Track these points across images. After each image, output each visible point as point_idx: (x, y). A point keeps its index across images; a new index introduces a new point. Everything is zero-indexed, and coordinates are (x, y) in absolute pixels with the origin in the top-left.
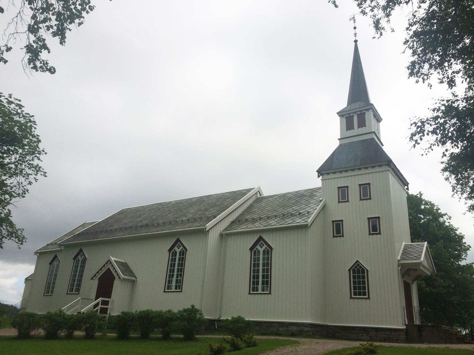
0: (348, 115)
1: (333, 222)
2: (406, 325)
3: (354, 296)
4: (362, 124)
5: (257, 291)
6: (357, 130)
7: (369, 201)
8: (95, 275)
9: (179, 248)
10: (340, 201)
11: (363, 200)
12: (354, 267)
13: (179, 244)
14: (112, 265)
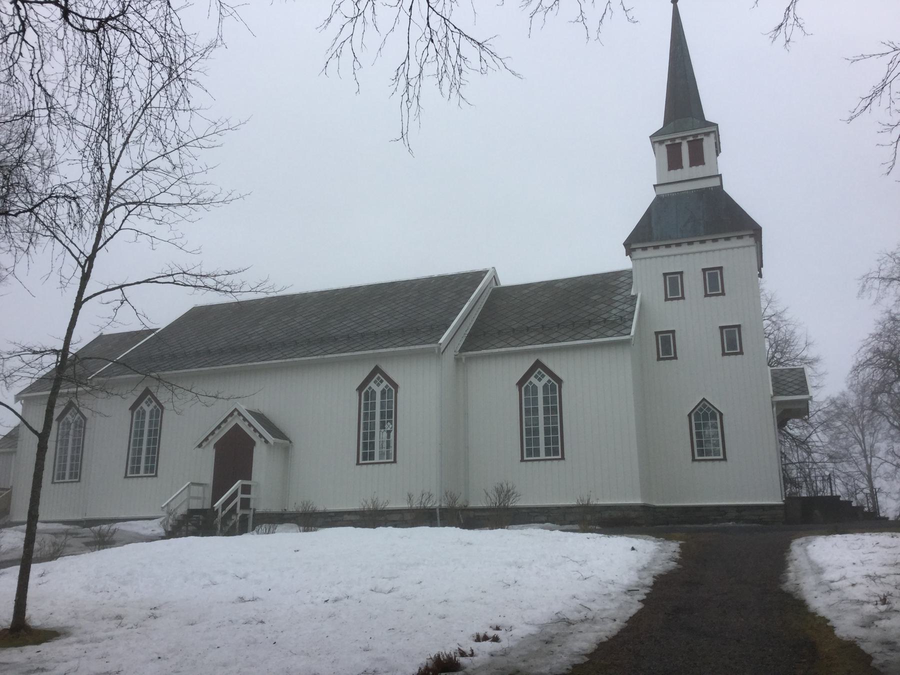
0: (671, 141)
1: (657, 333)
2: (784, 501)
3: (698, 456)
4: (697, 158)
5: (539, 456)
6: (688, 171)
7: (682, 301)
8: (206, 439)
9: (149, 405)
10: (669, 297)
11: (672, 299)
12: (697, 410)
13: (379, 377)
14: (245, 419)
